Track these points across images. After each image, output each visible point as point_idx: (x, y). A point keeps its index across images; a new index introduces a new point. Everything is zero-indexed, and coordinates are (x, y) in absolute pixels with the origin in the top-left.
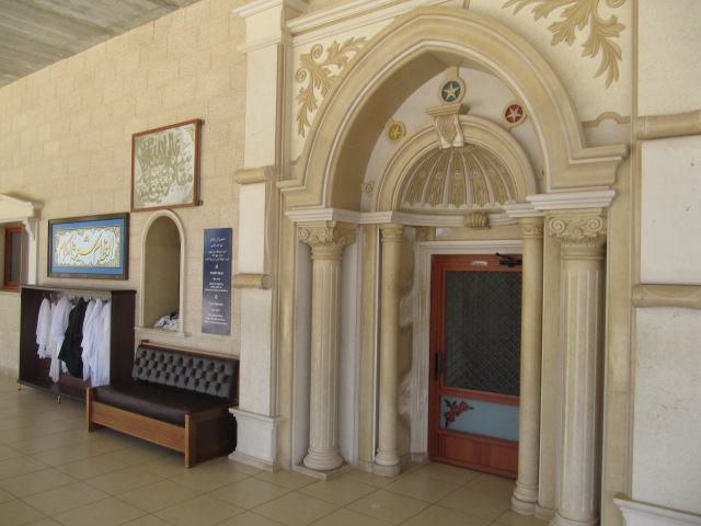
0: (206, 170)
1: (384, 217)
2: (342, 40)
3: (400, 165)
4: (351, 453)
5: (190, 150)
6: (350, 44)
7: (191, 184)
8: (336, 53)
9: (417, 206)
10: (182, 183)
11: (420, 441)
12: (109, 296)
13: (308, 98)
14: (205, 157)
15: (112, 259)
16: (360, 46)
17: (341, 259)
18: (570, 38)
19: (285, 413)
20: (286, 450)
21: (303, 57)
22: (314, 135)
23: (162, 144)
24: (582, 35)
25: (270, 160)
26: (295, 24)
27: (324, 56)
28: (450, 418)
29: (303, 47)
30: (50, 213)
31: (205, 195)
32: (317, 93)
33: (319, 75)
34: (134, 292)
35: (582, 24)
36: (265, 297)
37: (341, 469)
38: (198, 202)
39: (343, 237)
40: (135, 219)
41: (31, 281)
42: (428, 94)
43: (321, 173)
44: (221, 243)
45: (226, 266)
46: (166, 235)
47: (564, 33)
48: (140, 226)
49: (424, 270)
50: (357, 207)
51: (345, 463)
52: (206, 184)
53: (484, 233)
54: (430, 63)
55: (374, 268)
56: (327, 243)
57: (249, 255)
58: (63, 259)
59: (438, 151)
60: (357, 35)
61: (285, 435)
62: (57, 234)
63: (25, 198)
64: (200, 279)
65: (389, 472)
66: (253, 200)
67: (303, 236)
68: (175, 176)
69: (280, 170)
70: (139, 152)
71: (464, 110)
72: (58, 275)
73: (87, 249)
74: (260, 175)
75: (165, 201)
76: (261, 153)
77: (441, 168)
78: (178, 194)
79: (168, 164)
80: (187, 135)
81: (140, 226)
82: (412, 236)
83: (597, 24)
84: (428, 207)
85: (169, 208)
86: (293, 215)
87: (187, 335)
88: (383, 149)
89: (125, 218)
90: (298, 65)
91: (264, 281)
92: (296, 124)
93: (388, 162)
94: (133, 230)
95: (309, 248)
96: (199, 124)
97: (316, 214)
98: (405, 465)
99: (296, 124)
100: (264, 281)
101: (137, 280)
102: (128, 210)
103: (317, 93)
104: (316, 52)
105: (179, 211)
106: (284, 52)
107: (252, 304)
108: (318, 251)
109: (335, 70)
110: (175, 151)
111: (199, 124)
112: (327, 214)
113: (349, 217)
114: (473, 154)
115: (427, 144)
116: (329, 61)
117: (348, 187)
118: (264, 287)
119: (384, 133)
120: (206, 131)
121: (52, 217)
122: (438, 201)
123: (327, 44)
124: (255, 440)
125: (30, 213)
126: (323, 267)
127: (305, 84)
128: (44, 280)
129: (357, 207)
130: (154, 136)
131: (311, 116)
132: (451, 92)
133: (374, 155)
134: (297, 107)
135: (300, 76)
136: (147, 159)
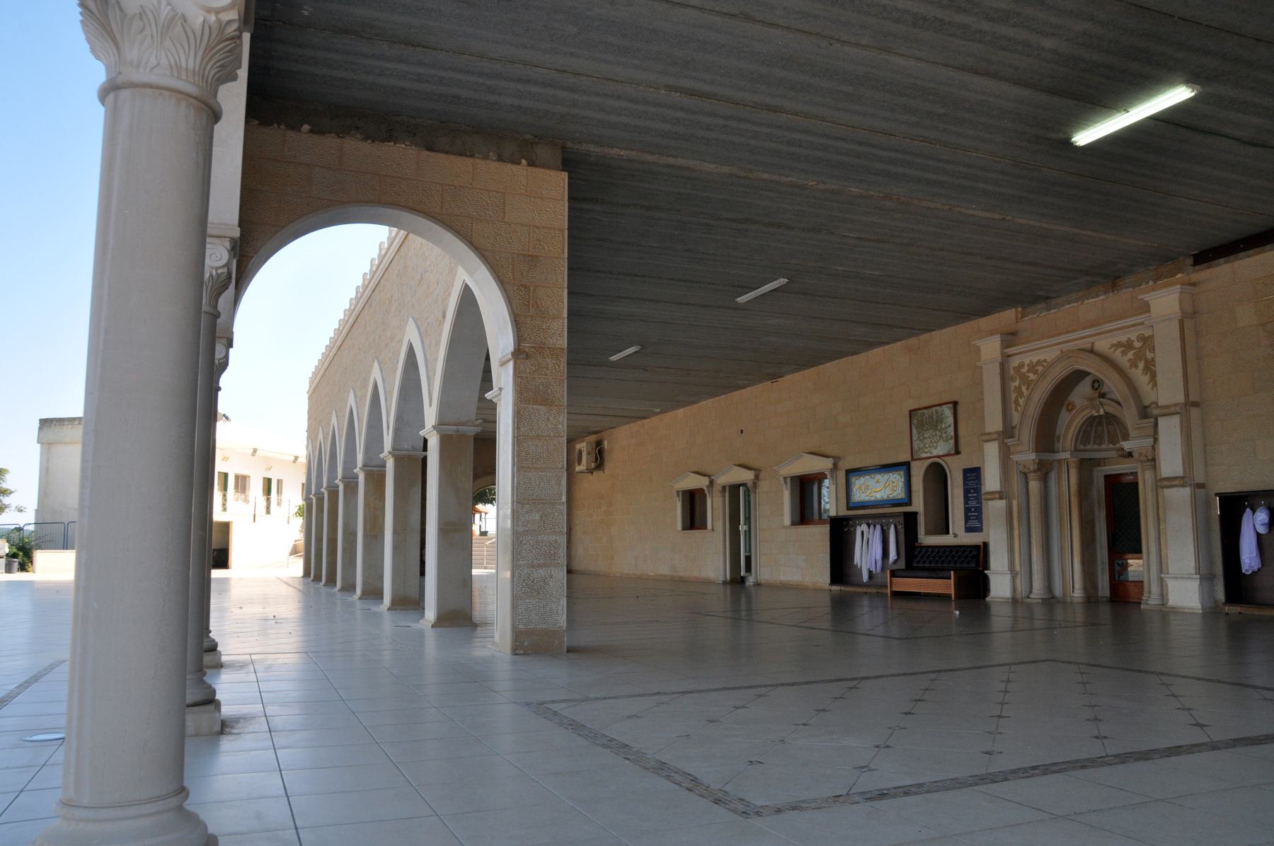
0: (961, 433)
1: (1066, 455)
2: (1035, 360)
3: (1075, 424)
4: (1058, 591)
5: (951, 420)
6: (1039, 362)
7: (952, 442)
8: (1032, 368)
9: (1089, 447)
12: (901, 520)
13: (1018, 389)
14: (960, 425)
16: (1040, 368)
17: (1045, 480)
18: (1136, 367)
19: (1018, 568)
21: (1015, 368)
23: (931, 416)
24: (1141, 365)
25: (1000, 428)
26: (1008, 351)
27: (1026, 368)
29: (1015, 362)
31: (962, 448)
33: (1024, 379)
34: (916, 513)
35: (1140, 359)
36: (1001, 504)
37: (1050, 601)
38: (957, 452)
39: (1044, 470)
40: (913, 464)
41: (833, 513)
42: (1084, 388)
43: (1027, 434)
44: (973, 476)
45: (978, 490)
46: (937, 475)
47: (1134, 364)
48: (918, 471)
49: (1099, 484)
51: (1053, 597)
52: (962, 442)
53: (1130, 459)
54: (1077, 377)
55: (1066, 483)
56: (1035, 471)
57: (991, 480)
58: (859, 495)
59: (1093, 418)
60: (1042, 357)
61: (1018, 582)
62: (853, 480)
63: (749, 468)
64: (962, 500)
65: (1080, 600)
66: (992, 452)
67: (1021, 468)
68: (941, 437)
69: (1008, 432)
71: (1102, 396)
73: (879, 488)
74: (994, 436)
75: (935, 452)
76: (994, 423)
78: (942, 448)
79: (936, 429)
80: (947, 412)
81: (918, 471)
84: (1096, 447)
85: (939, 457)
87: (956, 536)
88: (1065, 417)
90: (1012, 372)
92: (1013, 406)
93: (1069, 425)
95: (1025, 475)
96: (955, 404)
97: (1026, 456)
98: (1091, 600)
99: (1013, 406)
100: (1000, 495)
101: (918, 505)
102: (909, 459)
103: (1024, 389)
104: (1022, 365)
105: (946, 459)
106: (1003, 366)
107: (994, 509)
108: (1031, 476)
109: (1032, 376)
110: (940, 420)
111: (955, 404)
112: (1033, 456)
113: (1046, 456)
114: (1110, 419)
115: (1087, 413)
116: (1029, 371)
117: (1046, 439)
118: (1001, 498)
120: (960, 408)
121: (848, 467)
122: (1101, 444)
123: (1027, 362)
124: (1000, 586)
125: (831, 466)
126: (1034, 485)
127: (1017, 383)
128: (843, 512)
129: (1052, 450)
131: (1021, 401)
132: (1096, 385)
134: (1014, 396)
135: (1013, 379)
136: (921, 426)
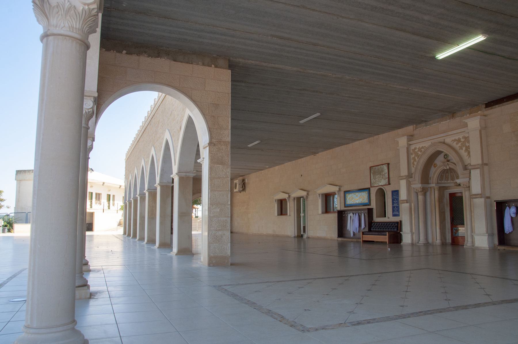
1: (434, 185)
2: (421, 146)
3: (437, 172)
4: (430, 241)
5: (387, 171)
7: (387, 180)
8: (420, 150)
9: (443, 182)
10: (385, 179)
11: (449, 240)
13: (414, 158)
15: (366, 201)
16: (423, 150)
17: (425, 195)
18: (462, 149)
19: (414, 231)
20: (414, 239)
22: (416, 168)
24: (464, 148)
25: (406, 174)
27: (417, 150)
28: (456, 233)
30: (344, 189)
31: (391, 182)
32: (416, 158)
33: (417, 154)
37: (427, 244)
38: (389, 184)
39: (424, 191)
40: (371, 189)
42: (441, 158)
43: (418, 177)
44: (396, 193)
46: (381, 193)
47: (461, 148)
48: (373, 191)
50: (428, 183)
52: (391, 179)
54: (438, 153)
55: (434, 196)
56: (421, 192)
57: (403, 195)
58: (349, 201)
59: (445, 170)
61: (414, 236)
62: (347, 195)
63: (305, 190)
64: (391, 203)
65: (439, 244)
66: (403, 184)
68: (383, 178)
69: (410, 176)
70: (372, 171)
72: (348, 207)
73: (357, 199)
74: (404, 177)
75: (380, 184)
76: (404, 172)
77: (447, 172)
78: (383, 182)
79: (381, 175)
80: (385, 167)
81: (373, 191)
82: (441, 189)
83: (466, 147)
85: (382, 186)
86: (413, 186)
87: (389, 218)
88: (433, 169)
89: (368, 189)
90: (412, 151)
91: (407, 201)
92: (412, 165)
93: (434, 173)
94: (371, 192)
96: (388, 164)
97: (417, 185)
98: (444, 244)
99: (412, 165)
100: (407, 201)
101: (373, 205)
103: (416, 158)
104: (415, 149)
106: (408, 149)
107: (404, 207)
108: (419, 194)
109: (419, 153)
110: (382, 171)
111: (388, 164)
112: (420, 185)
116: (418, 151)
117: (425, 178)
118: (407, 203)
119: (433, 166)
120: (390, 166)
121: (345, 190)
122: (448, 180)
123: (418, 147)
124: (407, 238)
126: (421, 197)
127: (413, 156)
128: (343, 208)
130: (376, 167)
131: (415, 163)
132: (446, 157)
133: (431, 172)
134: (412, 161)
135: (412, 154)
